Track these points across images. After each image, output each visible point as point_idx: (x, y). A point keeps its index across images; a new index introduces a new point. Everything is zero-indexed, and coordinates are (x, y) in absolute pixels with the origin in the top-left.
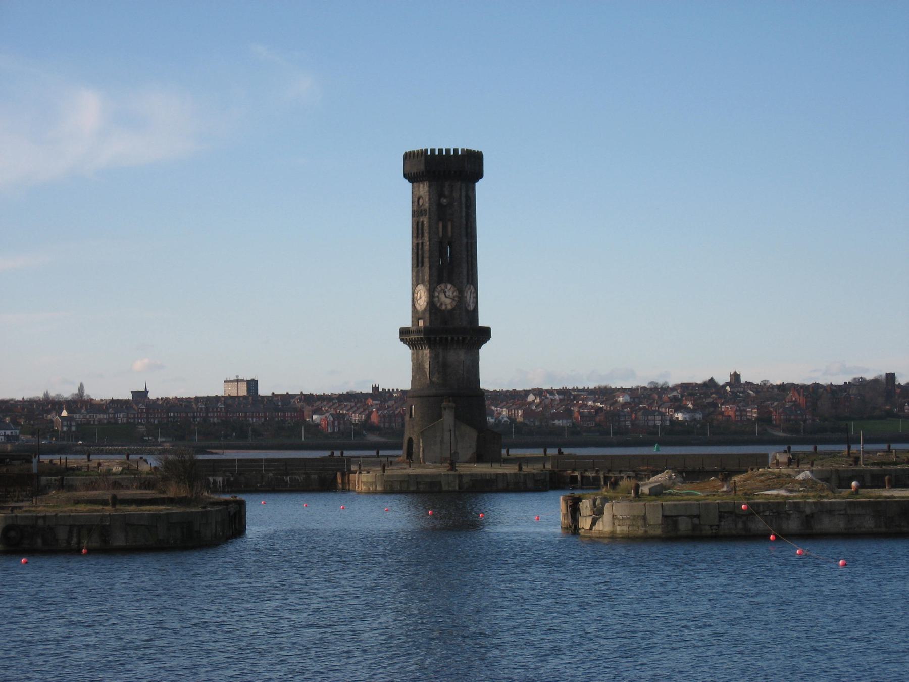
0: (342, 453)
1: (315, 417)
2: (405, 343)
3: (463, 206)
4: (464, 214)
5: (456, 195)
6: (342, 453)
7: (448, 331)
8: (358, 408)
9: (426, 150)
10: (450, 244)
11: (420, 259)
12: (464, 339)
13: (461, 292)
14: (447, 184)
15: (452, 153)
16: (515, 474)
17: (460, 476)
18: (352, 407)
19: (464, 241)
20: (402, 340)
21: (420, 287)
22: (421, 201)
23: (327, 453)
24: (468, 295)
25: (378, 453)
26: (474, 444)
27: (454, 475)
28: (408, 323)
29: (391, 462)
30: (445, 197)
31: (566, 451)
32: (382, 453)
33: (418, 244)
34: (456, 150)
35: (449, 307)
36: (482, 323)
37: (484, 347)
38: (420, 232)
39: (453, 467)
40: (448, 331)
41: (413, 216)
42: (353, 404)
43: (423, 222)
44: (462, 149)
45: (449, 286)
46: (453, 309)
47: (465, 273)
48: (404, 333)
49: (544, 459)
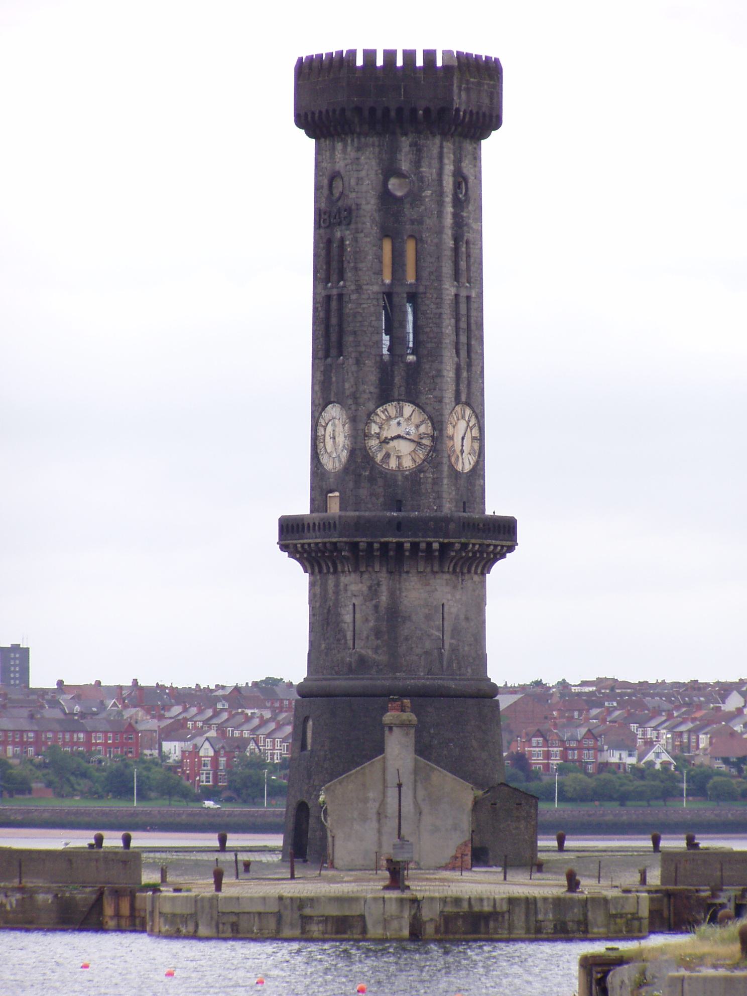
0: (127, 840)
1: (167, 746)
2: (291, 555)
3: (448, 199)
4: (448, 220)
5: (428, 171)
6: (127, 840)
7: (396, 535)
8: (279, 727)
9: (352, 53)
10: (413, 298)
11: (334, 337)
12: (444, 548)
13: (438, 424)
14: (405, 143)
15: (420, 62)
16: (558, 902)
17: (415, 902)
18: (263, 722)
20: (284, 547)
21: (333, 411)
22: (338, 184)
23: (81, 840)
24: (458, 429)
25: (223, 840)
26: (466, 822)
27: (401, 901)
28: (301, 506)
29: (247, 865)
30: (400, 175)
31: (706, 843)
32: (234, 840)
33: (328, 298)
34: (430, 55)
35: (408, 463)
36: (495, 505)
37: (499, 567)
38: (334, 264)
39: (397, 875)
40: (396, 535)
41: (318, 225)
42: (267, 714)
43: (342, 240)
44: (447, 53)
45: (408, 409)
46: (420, 469)
47: (449, 374)
48: (291, 532)
49: (627, 859)
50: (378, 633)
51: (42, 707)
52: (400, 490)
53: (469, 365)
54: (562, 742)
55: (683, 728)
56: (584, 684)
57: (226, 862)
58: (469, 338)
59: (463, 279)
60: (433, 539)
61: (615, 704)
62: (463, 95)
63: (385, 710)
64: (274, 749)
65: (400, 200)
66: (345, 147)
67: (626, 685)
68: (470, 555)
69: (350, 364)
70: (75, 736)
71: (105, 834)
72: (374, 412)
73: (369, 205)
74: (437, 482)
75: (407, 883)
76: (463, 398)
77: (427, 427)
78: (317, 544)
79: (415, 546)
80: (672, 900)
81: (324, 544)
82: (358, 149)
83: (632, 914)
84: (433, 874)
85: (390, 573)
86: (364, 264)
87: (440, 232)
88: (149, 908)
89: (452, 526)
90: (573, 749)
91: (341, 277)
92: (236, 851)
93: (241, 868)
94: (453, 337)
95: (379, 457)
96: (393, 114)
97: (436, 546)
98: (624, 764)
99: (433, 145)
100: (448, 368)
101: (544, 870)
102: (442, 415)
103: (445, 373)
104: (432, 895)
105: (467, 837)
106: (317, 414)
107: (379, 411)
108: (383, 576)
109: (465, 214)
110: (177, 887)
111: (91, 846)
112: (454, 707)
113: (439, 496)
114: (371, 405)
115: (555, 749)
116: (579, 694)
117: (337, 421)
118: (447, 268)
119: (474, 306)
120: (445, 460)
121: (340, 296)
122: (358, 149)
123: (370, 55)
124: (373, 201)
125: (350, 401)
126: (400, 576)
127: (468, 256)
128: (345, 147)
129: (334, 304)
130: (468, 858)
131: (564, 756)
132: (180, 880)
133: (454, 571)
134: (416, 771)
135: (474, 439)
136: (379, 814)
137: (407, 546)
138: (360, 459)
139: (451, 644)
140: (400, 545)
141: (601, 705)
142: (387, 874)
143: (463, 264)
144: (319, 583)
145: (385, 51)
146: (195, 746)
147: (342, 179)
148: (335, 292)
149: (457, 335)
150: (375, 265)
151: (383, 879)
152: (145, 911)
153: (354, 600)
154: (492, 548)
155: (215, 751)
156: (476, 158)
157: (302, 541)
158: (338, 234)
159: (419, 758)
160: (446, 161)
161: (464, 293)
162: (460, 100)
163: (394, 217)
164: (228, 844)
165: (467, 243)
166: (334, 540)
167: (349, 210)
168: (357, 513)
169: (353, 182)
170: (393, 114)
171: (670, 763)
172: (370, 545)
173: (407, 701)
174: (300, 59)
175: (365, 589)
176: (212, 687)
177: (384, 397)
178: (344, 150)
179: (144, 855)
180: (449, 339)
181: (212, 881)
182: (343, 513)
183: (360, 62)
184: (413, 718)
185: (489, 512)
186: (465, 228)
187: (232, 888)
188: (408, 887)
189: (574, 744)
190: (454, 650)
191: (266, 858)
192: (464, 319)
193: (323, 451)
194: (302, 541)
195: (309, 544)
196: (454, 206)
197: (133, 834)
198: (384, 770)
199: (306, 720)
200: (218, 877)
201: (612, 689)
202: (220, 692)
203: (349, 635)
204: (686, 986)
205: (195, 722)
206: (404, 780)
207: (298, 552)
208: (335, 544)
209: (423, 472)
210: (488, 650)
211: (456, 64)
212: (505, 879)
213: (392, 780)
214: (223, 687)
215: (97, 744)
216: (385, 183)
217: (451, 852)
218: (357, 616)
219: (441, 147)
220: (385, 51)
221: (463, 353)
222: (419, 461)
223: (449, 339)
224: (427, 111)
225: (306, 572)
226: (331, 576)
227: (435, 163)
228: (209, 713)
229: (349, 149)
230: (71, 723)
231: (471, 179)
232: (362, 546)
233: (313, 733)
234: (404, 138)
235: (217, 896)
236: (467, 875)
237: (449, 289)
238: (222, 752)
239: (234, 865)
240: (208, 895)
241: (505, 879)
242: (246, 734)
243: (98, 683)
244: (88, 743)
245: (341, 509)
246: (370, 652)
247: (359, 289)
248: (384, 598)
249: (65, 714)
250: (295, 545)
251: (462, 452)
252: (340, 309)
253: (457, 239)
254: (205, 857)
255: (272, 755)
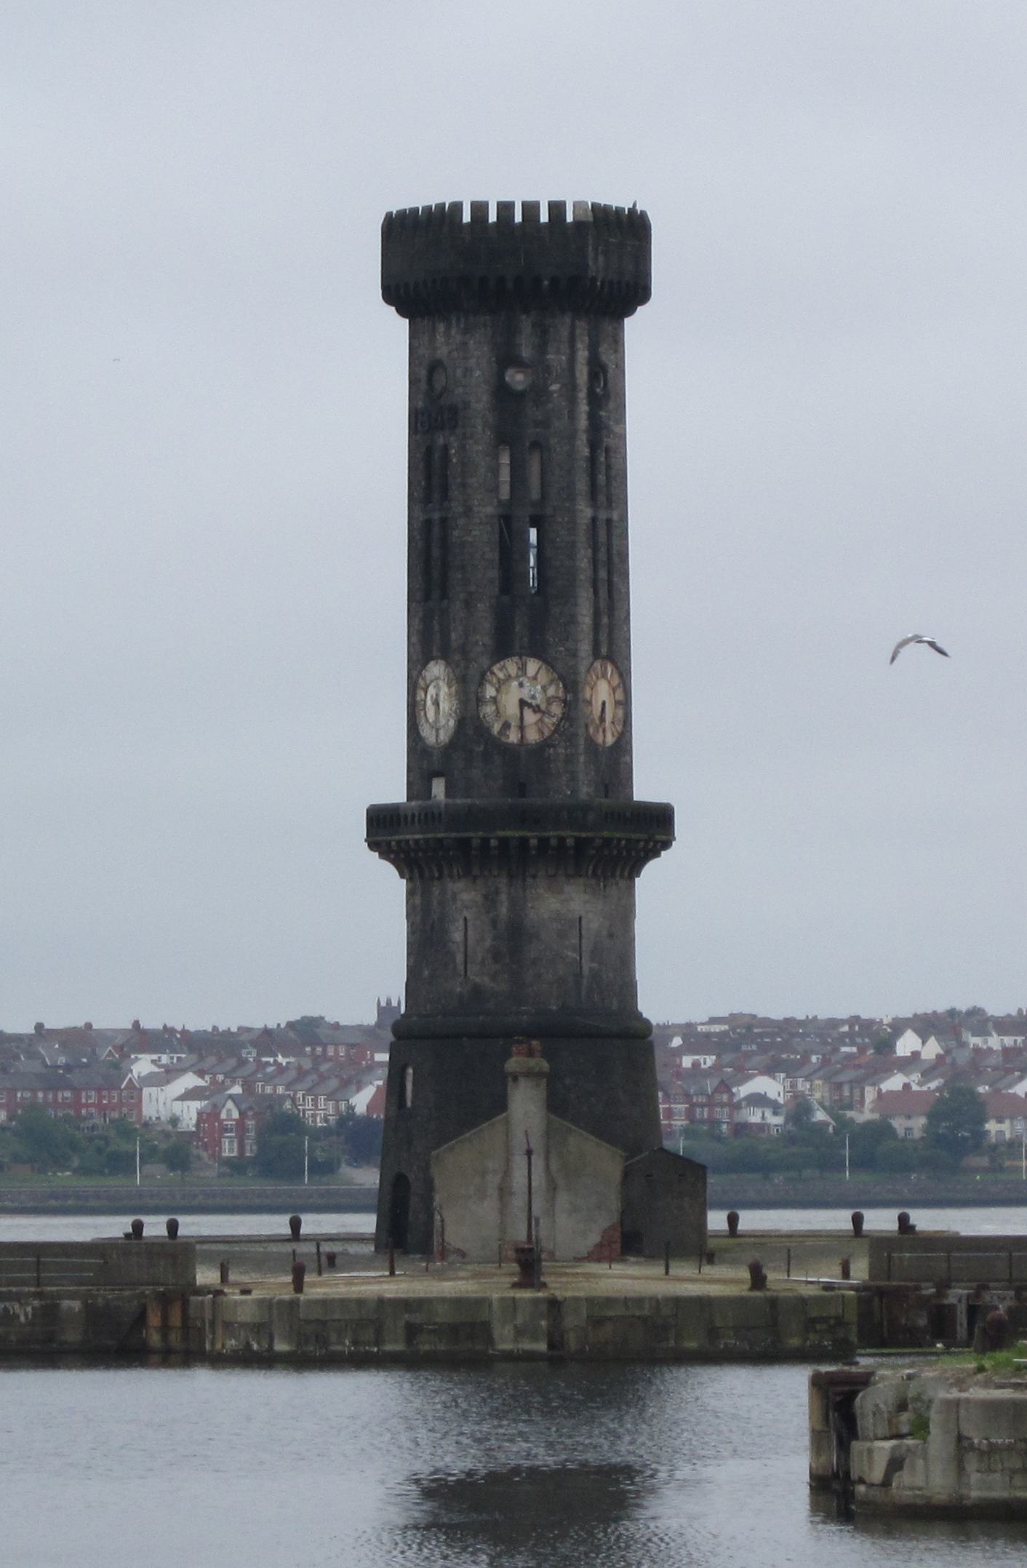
2: (383, 855)
3: (582, 394)
4: (583, 422)
5: (556, 358)
7: (519, 822)
8: (323, 1078)
13: (571, 686)
14: (526, 324)
19: (585, 512)
20: (373, 845)
21: (436, 670)
24: (602, 692)
27: (536, 1302)
28: (395, 791)
29: (332, 1258)
30: (518, 363)
33: (428, 524)
35: (533, 736)
36: (645, 789)
40: (519, 822)
42: (307, 1064)
43: (446, 448)
45: (533, 666)
46: (545, 744)
47: (586, 620)
50: (496, 956)
51: (17, 1057)
52: (523, 767)
53: (611, 609)
54: (688, 1097)
55: (841, 1078)
56: (713, 1021)
57: (307, 1255)
58: (610, 573)
59: (602, 498)
60: (529, 834)
61: (754, 1047)
62: (601, 259)
63: (507, 1055)
64: (317, 1109)
65: (521, 395)
66: (448, 328)
67: (767, 1022)
68: (615, 852)
69: (457, 608)
70: (60, 1095)
71: (145, 1219)
72: (489, 669)
73: (480, 401)
74: (570, 759)
75: (542, 1279)
76: (604, 650)
77: (557, 690)
78: (417, 841)
79: (544, 842)
80: (885, 1300)
81: (427, 841)
82: (466, 331)
83: (836, 1318)
84: (573, 1267)
85: (511, 877)
86: (474, 480)
87: (572, 436)
88: (208, 1315)
89: (591, 817)
90: (702, 1106)
91: (445, 496)
92: (318, 1240)
93: (324, 1260)
94: (589, 573)
95: (496, 728)
96: (510, 285)
97: (570, 842)
98: (769, 1125)
99: (562, 324)
100: (585, 612)
101: (716, 1260)
102: (576, 673)
103: (580, 619)
104: (577, 1294)
105: (615, 1218)
106: (415, 673)
107: (495, 669)
108: (502, 882)
109: (603, 413)
110: (246, 1288)
111: (127, 1236)
112: (600, 1050)
113: (573, 778)
114: (485, 661)
115: (679, 1106)
116: (708, 1035)
117: (441, 683)
118: (582, 485)
119: (616, 532)
120: (581, 731)
121: (444, 521)
122: (466, 331)
123: (479, 209)
124: (485, 398)
125: (457, 657)
126: (524, 880)
127: (609, 467)
128: (448, 328)
129: (436, 530)
130: (618, 1246)
131: (690, 1114)
132: (245, 1279)
133: (595, 874)
134: (549, 1133)
135: (617, 703)
136: (501, 1189)
137: (533, 842)
138: (470, 727)
139: (591, 969)
140: (524, 842)
141: (738, 1048)
142: (515, 1267)
143: (601, 478)
144: (419, 892)
145: (499, 204)
146: (215, 1106)
147: (445, 370)
148: (436, 516)
149: (595, 570)
150: (489, 476)
151: (511, 1274)
152: (203, 1320)
153: (466, 913)
154: (642, 843)
155: (240, 1114)
156: (617, 342)
157: (397, 837)
158: (441, 441)
159: (552, 1116)
160: (579, 345)
161: (603, 515)
162: (597, 265)
163: (514, 418)
164: (305, 1230)
165: (607, 450)
166: (440, 835)
167: (454, 410)
168: (469, 801)
169: (459, 373)
170: (510, 285)
171: (828, 1124)
172: (485, 841)
173: (535, 1043)
174: (389, 216)
175: (479, 898)
176: (234, 1029)
177: (502, 649)
178: (447, 333)
179: (198, 1247)
180: (584, 576)
181: (289, 1279)
182: (450, 801)
183: (467, 218)
184: (545, 1066)
185: (636, 798)
186: (605, 432)
187: (320, 1287)
188: (544, 1285)
189: (702, 1099)
190: (595, 975)
191: (354, 1249)
192: (603, 550)
193: (423, 721)
194: (397, 837)
195: (407, 841)
196: (590, 404)
197: (182, 1219)
198: (507, 1133)
199: (403, 1070)
200: (299, 1275)
201: (749, 1028)
202: (244, 1037)
203: (460, 958)
204: (962, 1412)
205: (215, 1075)
206: (534, 1146)
207: (392, 852)
208: (440, 840)
209: (554, 746)
210: (639, 976)
211: (591, 219)
212: (667, 1273)
213: (519, 1142)
214: (249, 1030)
215: (87, 1106)
216: (501, 376)
217: (594, 1238)
218: (470, 932)
219: (573, 327)
220: (499, 204)
221: (603, 593)
222: (547, 733)
223: (584, 576)
224: (554, 281)
225: (402, 877)
226: (436, 882)
227: (565, 347)
228: (232, 1062)
229: (453, 332)
230: (53, 1080)
231: (611, 368)
232: (475, 843)
233: (414, 1084)
234: (524, 317)
235: (298, 1299)
236: (617, 1269)
237: (585, 512)
238: (250, 1113)
239: (316, 1257)
240: (287, 1297)
241: (667, 1273)
242: (281, 1090)
243: (89, 1026)
244: (77, 1105)
245: (448, 794)
246: (486, 979)
247: (468, 511)
248: (504, 910)
249: (46, 1066)
250: (389, 843)
251: (602, 719)
252: (444, 539)
253: (594, 445)
254: (274, 1248)
255: (314, 1116)
